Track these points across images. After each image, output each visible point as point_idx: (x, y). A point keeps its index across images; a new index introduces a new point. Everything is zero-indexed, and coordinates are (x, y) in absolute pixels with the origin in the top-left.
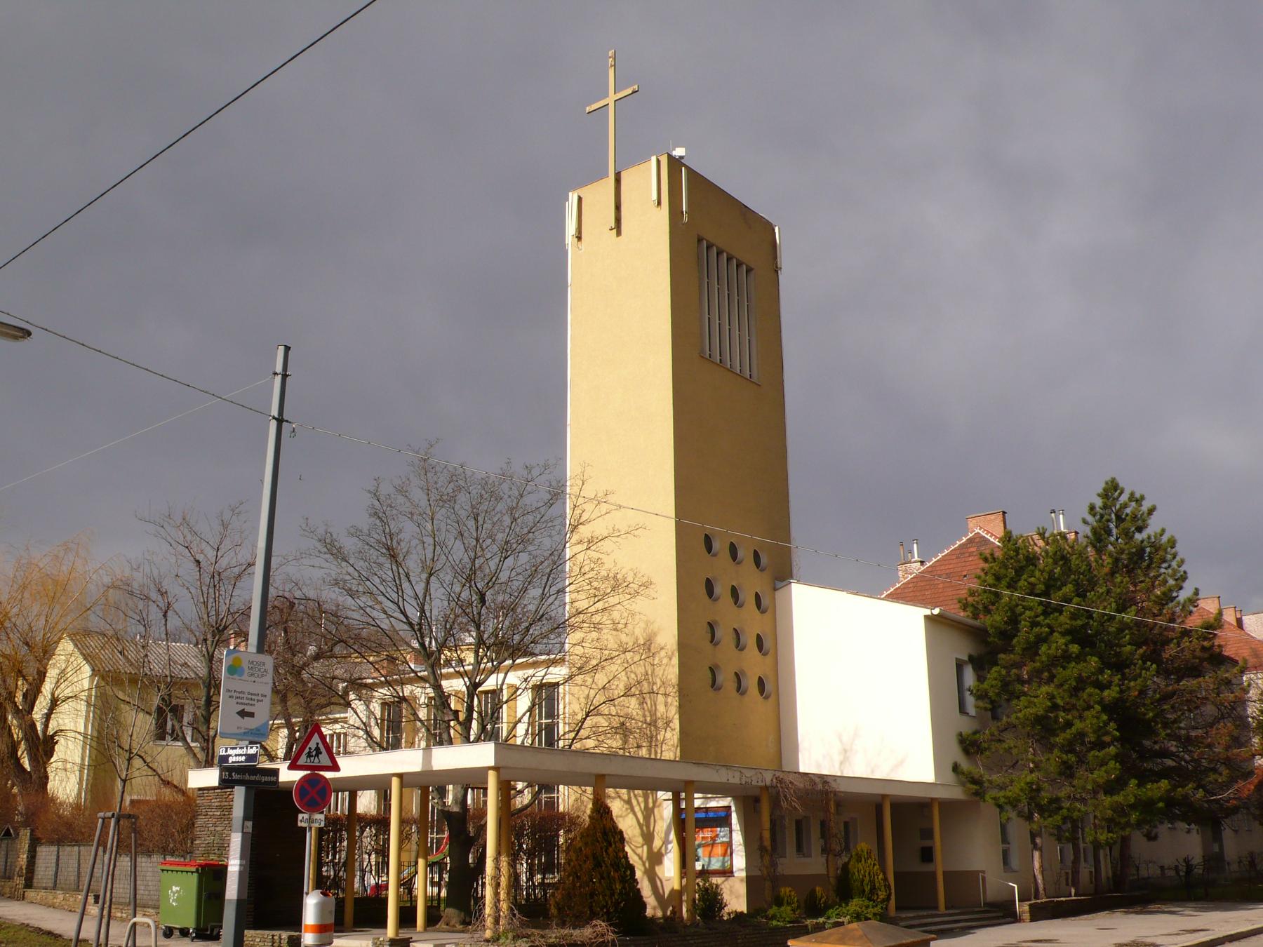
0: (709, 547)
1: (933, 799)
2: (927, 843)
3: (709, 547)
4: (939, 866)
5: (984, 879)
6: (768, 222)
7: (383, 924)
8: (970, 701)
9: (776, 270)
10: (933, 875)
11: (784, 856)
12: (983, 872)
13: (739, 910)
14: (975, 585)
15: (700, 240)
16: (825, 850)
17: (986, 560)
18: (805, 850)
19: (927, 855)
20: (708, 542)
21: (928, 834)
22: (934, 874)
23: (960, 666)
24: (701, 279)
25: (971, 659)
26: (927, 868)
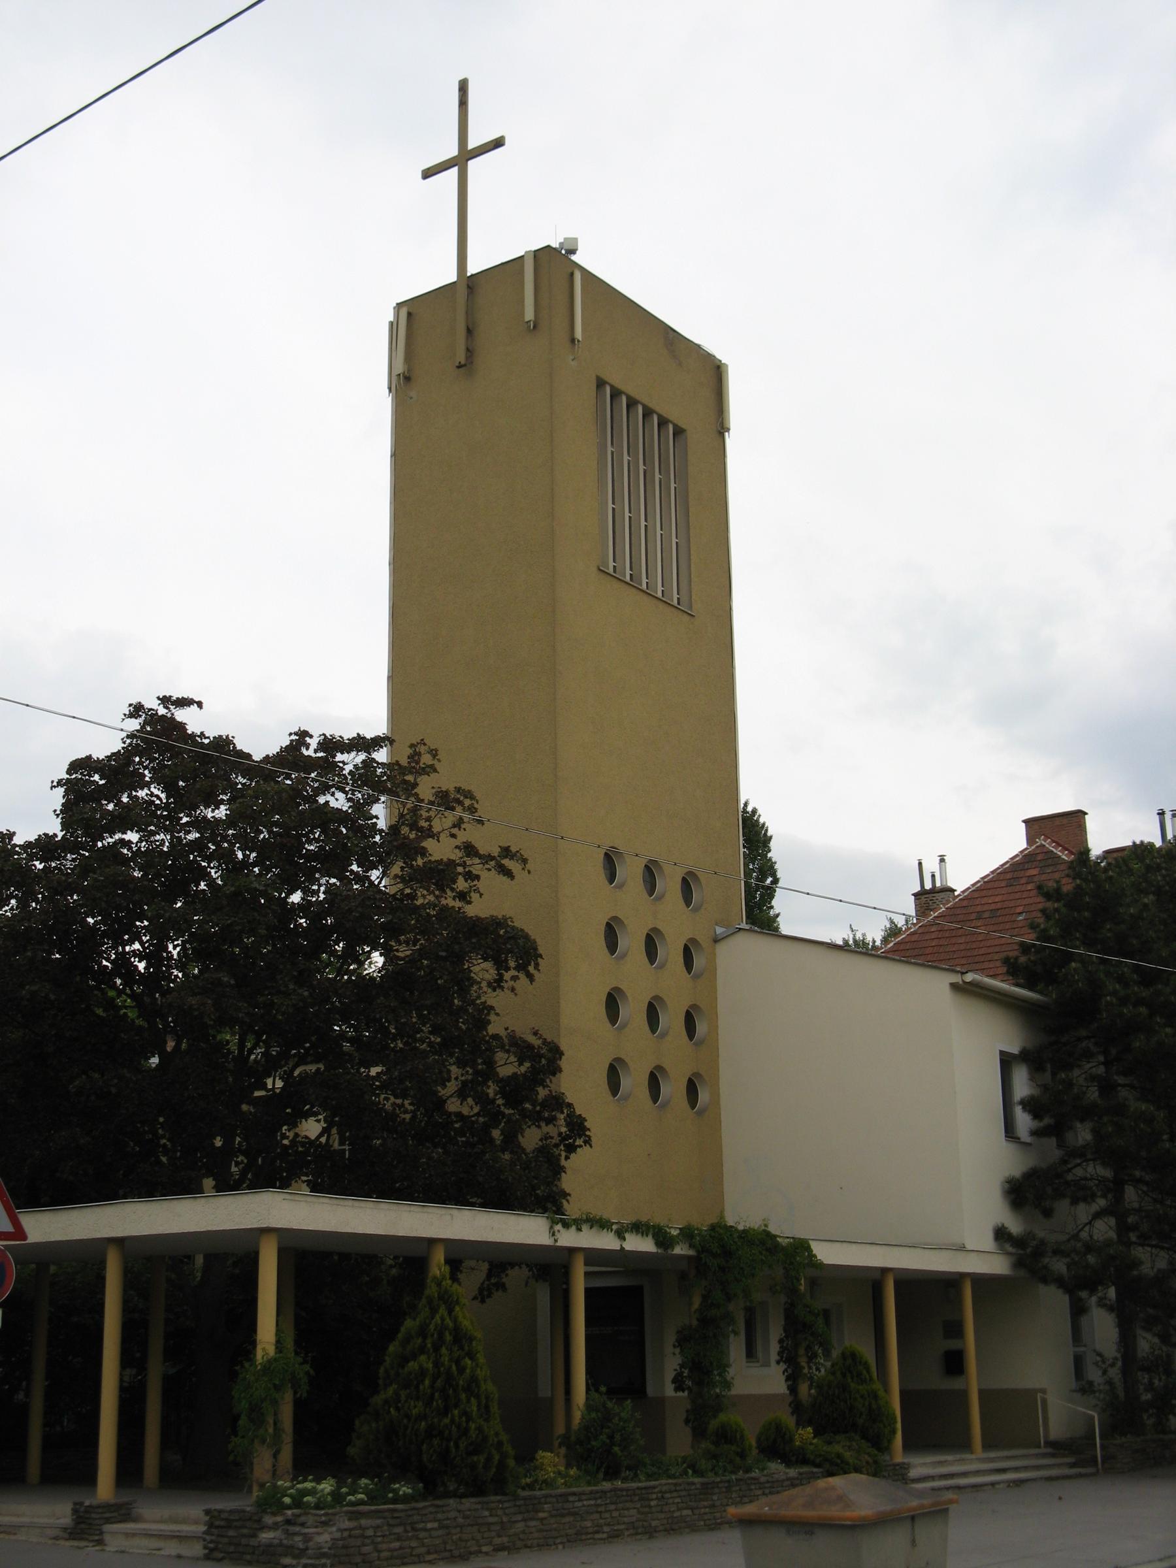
0: (612, 942)
1: (963, 1276)
2: (953, 1344)
3: (612, 942)
4: (973, 1381)
5: (1044, 1401)
6: (709, 357)
7: (89, 1478)
8: (1024, 1121)
9: (721, 429)
10: (962, 1396)
11: (461, 1272)
12: (1044, 1391)
13: (250, 716)
14: (1029, 938)
15: (601, 383)
16: (788, 1357)
17: (1048, 896)
18: (760, 1354)
19: (954, 1363)
20: (610, 862)
21: (955, 1329)
22: (964, 1395)
23: (1007, 1062)
24: (602, 448)
25: (1025, 1056)
26: (956, 1384)
